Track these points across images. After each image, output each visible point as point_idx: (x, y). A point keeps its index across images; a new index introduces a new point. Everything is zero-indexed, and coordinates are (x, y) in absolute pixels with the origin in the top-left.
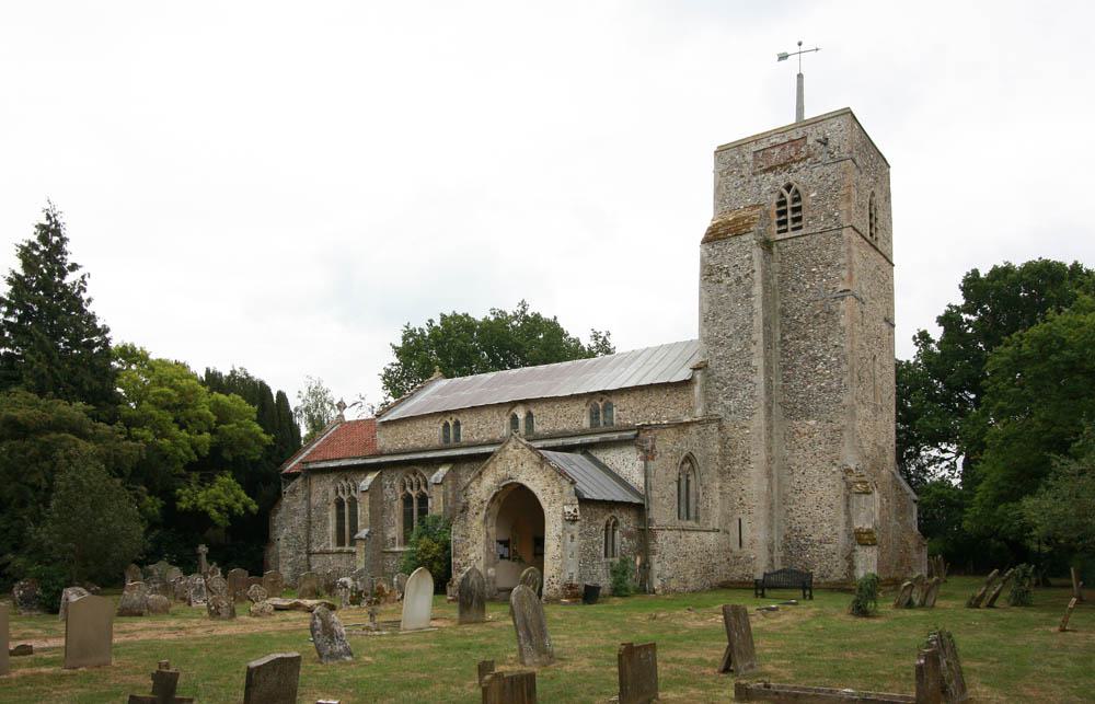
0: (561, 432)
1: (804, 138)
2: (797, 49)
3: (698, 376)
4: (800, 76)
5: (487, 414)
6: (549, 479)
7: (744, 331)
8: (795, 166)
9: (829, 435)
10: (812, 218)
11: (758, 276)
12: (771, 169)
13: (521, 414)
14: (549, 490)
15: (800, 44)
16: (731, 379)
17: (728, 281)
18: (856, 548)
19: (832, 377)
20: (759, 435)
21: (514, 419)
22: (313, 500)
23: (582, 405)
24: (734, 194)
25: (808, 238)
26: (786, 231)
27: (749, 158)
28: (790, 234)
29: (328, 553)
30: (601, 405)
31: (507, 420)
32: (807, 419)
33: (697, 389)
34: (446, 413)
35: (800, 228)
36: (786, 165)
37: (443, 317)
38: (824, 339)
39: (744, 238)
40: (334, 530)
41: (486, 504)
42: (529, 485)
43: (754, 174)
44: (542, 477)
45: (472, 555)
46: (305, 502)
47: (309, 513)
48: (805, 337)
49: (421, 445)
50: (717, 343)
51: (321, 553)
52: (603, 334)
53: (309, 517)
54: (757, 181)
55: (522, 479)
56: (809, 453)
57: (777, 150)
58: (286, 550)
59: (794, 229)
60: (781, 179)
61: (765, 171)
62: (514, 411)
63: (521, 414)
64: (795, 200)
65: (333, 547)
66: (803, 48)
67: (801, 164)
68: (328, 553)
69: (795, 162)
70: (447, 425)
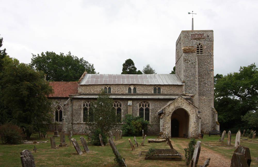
0: (145, 94)
1: (203, 34)
2: (192, 13)
3: (184, 84)
4: (193, 19)
5: (122, 87)
6: (192, 108)
7: (193, 75)
8: (201, 40)
9: (208, 100)
10: (205, 52)
11: (197, 63)
12: (195, 39)
13: (132, 88)
14: (192, 111)
15: (193, 12)
16: (191, 86)
17: (190, 63)
18: (216, 125)
19: (209, 88)
20: (197, 99)
21: (130, 89)
22: (74, 107)
23: (153, 87)
24: (186, 43)
25: (204, 56)
26: (199, 54)
27: (190, 35)
28: (200, 55)
29: (81, 124)
30: (157, 88)
32: (203, 96)
33: (184, 87)
34: (106, 85)
35: (202, 54)
36: (199, 39)
38: (208, 79)
39: (194, 54)
40: (83, 117)
41: (171, 113)
42: (186, 109)
43: (191, 39)
44: (190, 107)
45: (167, 126)
46: (71, 108)
47: (72, 111)
48: (203, 78)
49: (96, 93)
50: (187, 77)
53: (72, 112)
54: (192, 41)
55: (183, 107)
56: (204, 104)
57: (197, 35)
58: (66, 123)
59: (201, 54)
61: (194, 39)
62: (130, 86)
63: (132, 88)
64: (201, 47)
65: (82, 122)
66: (193, 13)
67: (202, 40)
68: (81, 124)
69: (201, 39)
70: (106, 88)
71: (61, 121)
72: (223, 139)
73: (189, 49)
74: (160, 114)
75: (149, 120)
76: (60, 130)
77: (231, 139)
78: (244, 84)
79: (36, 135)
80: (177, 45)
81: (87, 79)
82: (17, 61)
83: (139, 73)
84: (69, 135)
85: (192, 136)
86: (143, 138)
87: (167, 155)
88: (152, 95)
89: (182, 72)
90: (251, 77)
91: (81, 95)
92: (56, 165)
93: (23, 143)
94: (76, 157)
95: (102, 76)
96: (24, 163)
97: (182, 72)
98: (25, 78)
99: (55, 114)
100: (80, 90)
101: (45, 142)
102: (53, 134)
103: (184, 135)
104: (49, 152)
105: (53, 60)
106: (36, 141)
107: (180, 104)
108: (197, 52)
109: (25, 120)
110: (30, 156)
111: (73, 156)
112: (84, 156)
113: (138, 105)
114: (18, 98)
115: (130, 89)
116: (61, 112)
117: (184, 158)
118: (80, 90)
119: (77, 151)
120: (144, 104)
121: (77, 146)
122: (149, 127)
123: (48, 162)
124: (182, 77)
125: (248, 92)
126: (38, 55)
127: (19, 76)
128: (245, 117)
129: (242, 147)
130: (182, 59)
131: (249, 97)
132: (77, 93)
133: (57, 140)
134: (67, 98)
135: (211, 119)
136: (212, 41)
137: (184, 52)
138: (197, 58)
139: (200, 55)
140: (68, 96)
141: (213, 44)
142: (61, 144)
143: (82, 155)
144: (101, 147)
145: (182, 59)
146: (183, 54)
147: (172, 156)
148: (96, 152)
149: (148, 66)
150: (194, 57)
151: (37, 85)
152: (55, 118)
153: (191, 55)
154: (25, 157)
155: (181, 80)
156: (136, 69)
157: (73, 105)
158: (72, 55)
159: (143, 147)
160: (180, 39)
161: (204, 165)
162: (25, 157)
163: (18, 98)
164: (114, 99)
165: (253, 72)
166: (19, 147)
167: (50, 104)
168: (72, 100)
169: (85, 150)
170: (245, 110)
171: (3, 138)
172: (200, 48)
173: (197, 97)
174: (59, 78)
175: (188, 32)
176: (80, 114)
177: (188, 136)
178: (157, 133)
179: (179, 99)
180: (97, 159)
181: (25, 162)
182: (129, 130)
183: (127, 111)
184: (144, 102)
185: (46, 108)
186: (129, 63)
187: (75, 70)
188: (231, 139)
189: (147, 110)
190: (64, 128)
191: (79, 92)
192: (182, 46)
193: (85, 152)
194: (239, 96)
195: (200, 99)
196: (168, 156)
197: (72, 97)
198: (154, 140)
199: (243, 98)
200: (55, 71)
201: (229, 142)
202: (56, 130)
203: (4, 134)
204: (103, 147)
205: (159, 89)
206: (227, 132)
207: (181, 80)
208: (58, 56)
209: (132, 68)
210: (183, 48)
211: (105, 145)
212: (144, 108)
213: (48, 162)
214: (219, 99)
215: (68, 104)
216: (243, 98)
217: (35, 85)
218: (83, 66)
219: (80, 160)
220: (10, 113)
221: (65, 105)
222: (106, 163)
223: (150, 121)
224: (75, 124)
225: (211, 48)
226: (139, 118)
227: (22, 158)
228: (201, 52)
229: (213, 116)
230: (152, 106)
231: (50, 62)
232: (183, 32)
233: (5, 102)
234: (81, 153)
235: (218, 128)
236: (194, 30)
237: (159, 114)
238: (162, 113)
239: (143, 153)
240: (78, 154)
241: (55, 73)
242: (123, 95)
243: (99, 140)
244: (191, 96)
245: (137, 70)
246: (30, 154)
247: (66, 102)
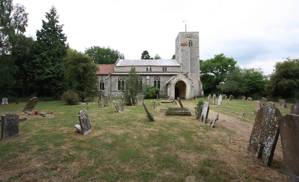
3: (181, 65)
4: (186, 25)
7: (187, 60)
11: (189, 52)
12: (188, 37)
13: (149, 68)
15: (184, 21)
21: (147, 69)
22: (112, 81)
23: (162, 68)
27: (185, 35)
28: (191, 47)
29: (116, 91)
30: (165, 68)
31: (146, 68)
33: (181, 67)
36: (190, 37)
37: (94, 47)
39: (187, 46)
41: (175, 84)
47: (111, 83)
51: (114, 91)
52: (123, 54)
55: (183, 80)
60: (190, 39)
63: (149, 68)
65: (117, 90)
68: (116, 91)
71: (103, 89)
72: (209, 100)
73: (184, 43)
74: (167, 85)
75: (160, 88)
76: (103, 96)
77: (215, 100)
78: (217, 65)
79: (88, 99)
80: (176, 41)
81: (120, 63)
82: (76, 51)
83: (152, 59)
84: (109, 99)
85: (188, 98)
86: (158, 100)
87: (187, 112)
88: (161, 72)
89: (180, 58)
90: (221, 61)
91: (116, 72)
92: (104, 120)
93: (79, 104)
94: (117, 114)
95: (129, 61)
96: (81, 121)
97: (180, 58)
98: (81, 61)
99: (99, 84)
100: (116, 70)
101: (94, 103)
102: (99, 98)
103: (183, 98)
104: (98, 111)
105: (98, 51)
106: (88, 103)
107: (180, 78)
108: (189, 45)
109: (81, 89)
110: (85, 115)
111: (114, 113)
112: (122, 114)
113: (153, 78)
114: (76, 74)
115: (147, 69)
116: (103, 84)
117: (193, 114)
118: (116, 70)
119: (117, 110)
120: (157, 78)
121: (117, 106)
122: (160, 93)
123: (98, 118)
124: (180, 61)
125: (220, 70)
126: (89, 48)
127: (77, 60)
128: (218, 86)
129: (269, 107)
130: (180, 49)
131: (220, 74)
132: (114, 71)
133: (102, 102)
134: (107, 75)
135: (198, 87)
136: (198, 38)
137: (181, 46)
138: (189, 49)
139: (191, 47)
140: (108, 74)
141: (199, 40)
142: (105, 105)
143: (121, 113)
144: (131, 106)
145: (180, 49)
146: (181, 47)
147: (185, 112)
148: (130, 110)
149: (157, 55)
150: (187, 48)
151: (89, 65)
152: (99, 88)
153: (185, 47)
154: (82, 116)
155: (179, 63)
156: (150, 57)
157: (111, 79)
158: (110, 48)
159: (160, 106)
160: (178, 37)
161: (214, 120)
162: (82, 116)
163: (76, 74)
164: (140, 75)
165: (223, 58)
166: (77, 107)
167: (97, 78)
168: (111, 76)
169: (122, 109)
170: (218, 82)
171: (66, 101)
172: (191, 43)
173: (189, 73)
174: (102, 62)
175: (183, 33)
176: (116, 84)
177: (185, 98)
178: (166, 97)
179: (180, 74)
180: (132, 115)
181: (82, 120)
182: (148, 95)
183: (146, 82)
184: (157, 77)
185: (94, 81)
186: (145, 53)
187: (112, 57)
188: (215, 100)
189: (159, 82)
190: (105, 94)
191: (115, 71)
192: (180, 42)
193: (122, 110)
194: (214, 73)
195: (191, 75)
196: (182, 112)
197: (111, 74)
198: (166, 101)
199: (217, 74)
200: (100, 58)
201: (213, 102)
202: (101, 96)
203: (67, 98)
204: (133, 107)
205: (166, 68)
206: (212, 96)
207: (179, 63)
208: (101, 48)
209: (147, 56)
210: (180, 43)
211: (134, 105)
212: (157, 81)
213: (98, 118)
214: (202, 75)
215: (108, 79)
216: (217, 74)
217: (87, 65)
218: (117, 55)
219: (120, 116)
220: (70, 85)
221: (106, 79)
222: (139, 119)
223: (161, 89)
224: (112, 91)
225: (198, 43)
226: (154, 87)
227: (79, 117)
228: (191, 44)
229: (200, 85)
230: (162, 79)
231: (97, 52)
232: (180, 33)
233: (67, 77)
234: (120, 111)
235: (203, 93)
236: (187, 31)
237: (166, 85)
238: (169, 84)
239: (162, 110)
240: (118, 112)
241: (100, 60)
242: (143, 72)
243: (131, 102)
244: (187, 73)
245: (151, 58)
246: (86, 113)
247: (107, 77)
